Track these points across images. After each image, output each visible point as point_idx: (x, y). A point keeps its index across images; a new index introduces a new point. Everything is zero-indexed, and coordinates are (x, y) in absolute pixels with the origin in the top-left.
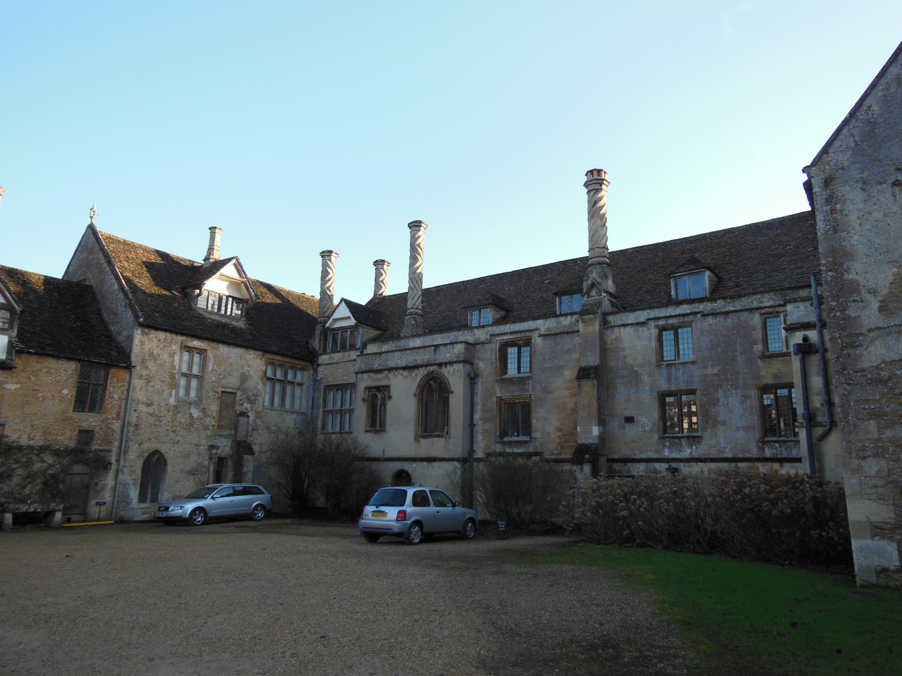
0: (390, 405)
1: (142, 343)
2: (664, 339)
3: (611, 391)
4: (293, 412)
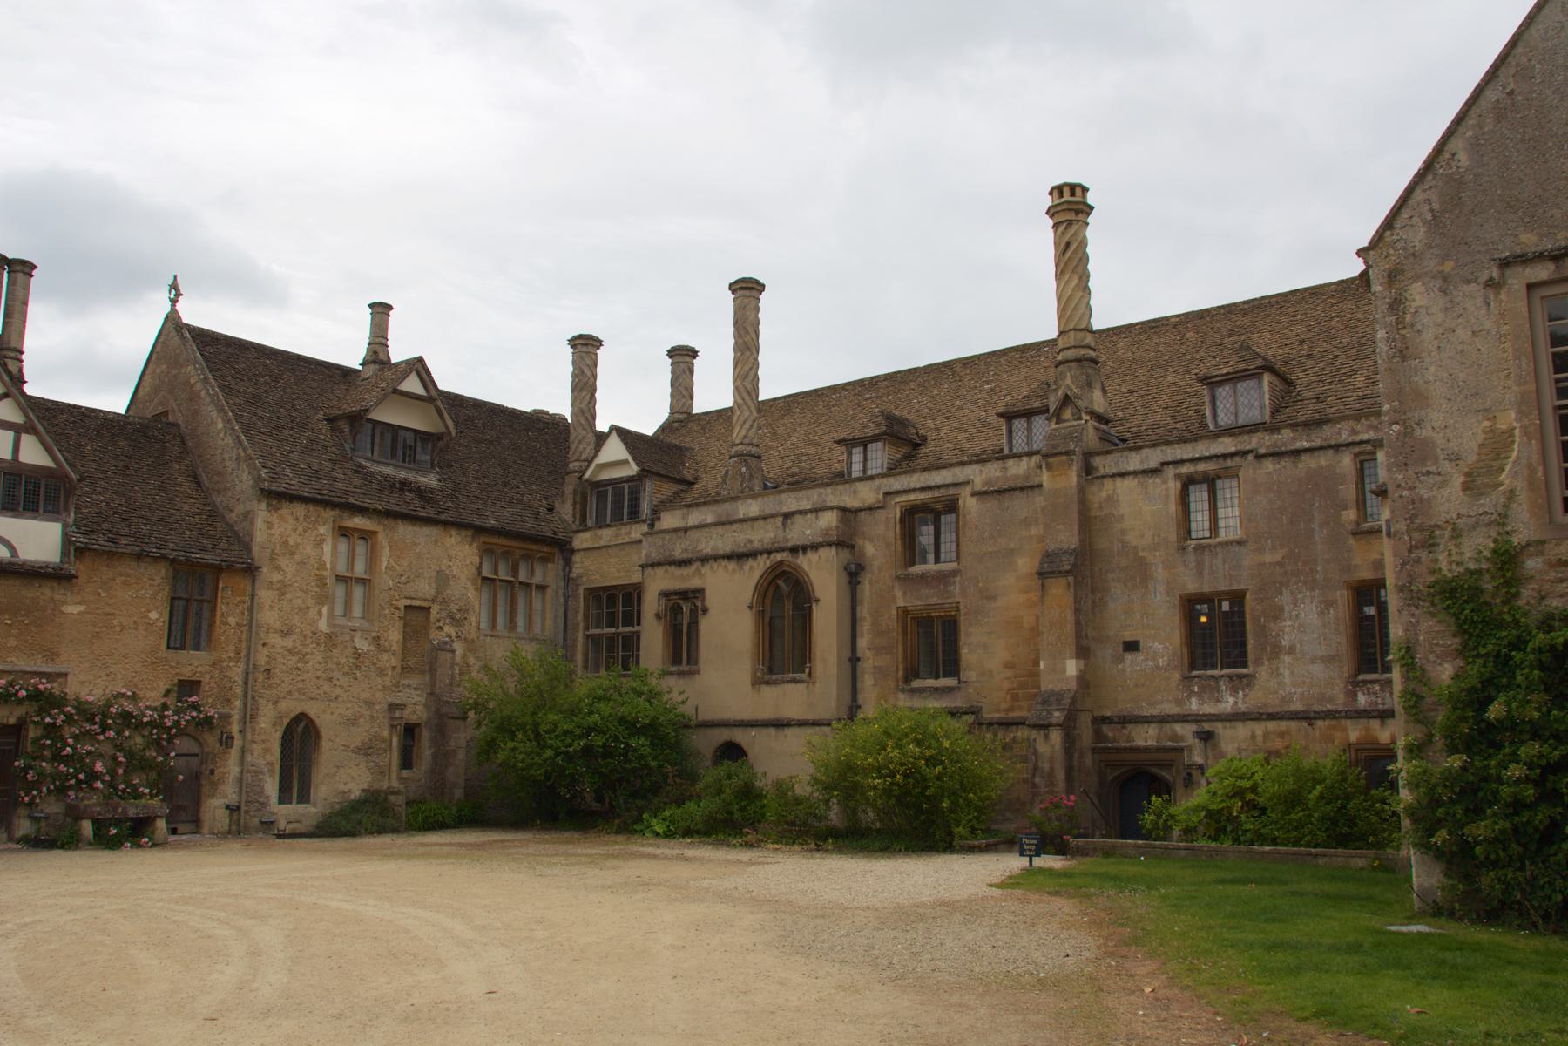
0: (705, 624)
1: (270, 525)
2: (1191, 499)
3: (1099, 595)
4: (531, 640)
